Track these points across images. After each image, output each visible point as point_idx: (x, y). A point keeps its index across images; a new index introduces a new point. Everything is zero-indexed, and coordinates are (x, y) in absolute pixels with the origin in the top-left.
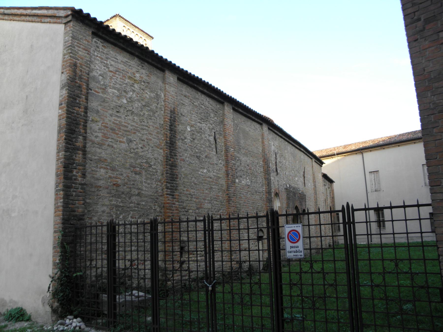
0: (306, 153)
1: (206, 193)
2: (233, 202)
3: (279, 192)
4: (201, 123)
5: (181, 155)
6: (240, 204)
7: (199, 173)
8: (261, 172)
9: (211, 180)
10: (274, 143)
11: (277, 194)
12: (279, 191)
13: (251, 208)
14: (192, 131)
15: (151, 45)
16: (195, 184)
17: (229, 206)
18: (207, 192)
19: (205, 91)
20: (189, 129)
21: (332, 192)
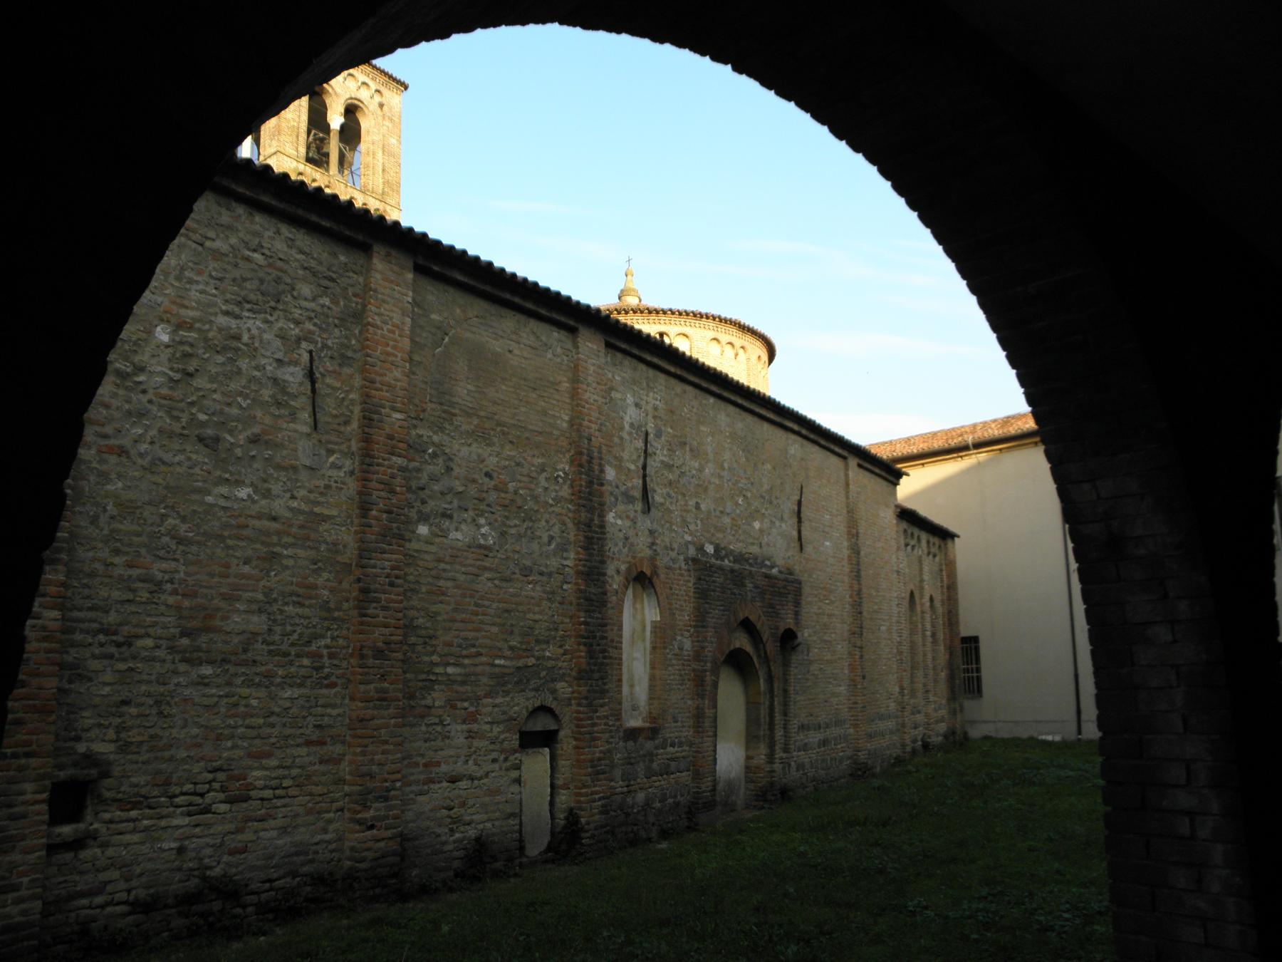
0: (812, 436)
1: (243, 576)
2: (384, 608)
3: (655, 573)
4: (237, 317)
5: (109, 429)
6: (433, 617)
7: (209, 499)
8: (558, 500)
9: (275, 525)
10: (638, 401)
11: (642, 580)
12: (655, 567)
13: (495, 629)
14: (181, 343)
15: (775, 383)
16: (181, 541)
17: (362, 623)
18: (246, 569)
19: (265, 198)
20: (165, 338)
21: (949, 569)
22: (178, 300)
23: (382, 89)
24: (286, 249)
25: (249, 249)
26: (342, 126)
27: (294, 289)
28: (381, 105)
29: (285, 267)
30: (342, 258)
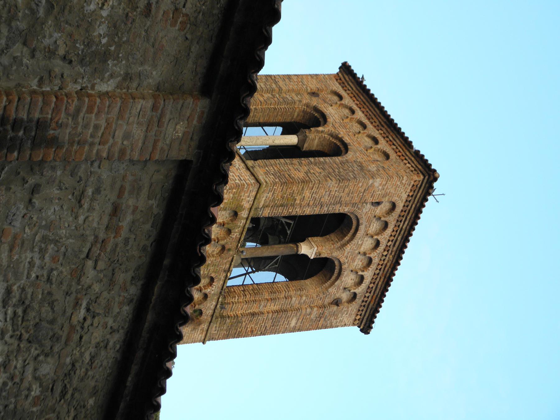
19: (150, 317)
22: (18, 242)
23: (358, 301)
24: (94, 342)
25: (88, 304)
26: (305, 257)
27: (47, 355)
28: (337, 302)
29: (72, 344)
30: (91, 402)
